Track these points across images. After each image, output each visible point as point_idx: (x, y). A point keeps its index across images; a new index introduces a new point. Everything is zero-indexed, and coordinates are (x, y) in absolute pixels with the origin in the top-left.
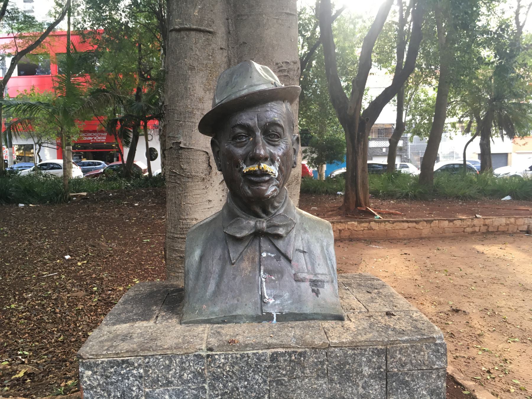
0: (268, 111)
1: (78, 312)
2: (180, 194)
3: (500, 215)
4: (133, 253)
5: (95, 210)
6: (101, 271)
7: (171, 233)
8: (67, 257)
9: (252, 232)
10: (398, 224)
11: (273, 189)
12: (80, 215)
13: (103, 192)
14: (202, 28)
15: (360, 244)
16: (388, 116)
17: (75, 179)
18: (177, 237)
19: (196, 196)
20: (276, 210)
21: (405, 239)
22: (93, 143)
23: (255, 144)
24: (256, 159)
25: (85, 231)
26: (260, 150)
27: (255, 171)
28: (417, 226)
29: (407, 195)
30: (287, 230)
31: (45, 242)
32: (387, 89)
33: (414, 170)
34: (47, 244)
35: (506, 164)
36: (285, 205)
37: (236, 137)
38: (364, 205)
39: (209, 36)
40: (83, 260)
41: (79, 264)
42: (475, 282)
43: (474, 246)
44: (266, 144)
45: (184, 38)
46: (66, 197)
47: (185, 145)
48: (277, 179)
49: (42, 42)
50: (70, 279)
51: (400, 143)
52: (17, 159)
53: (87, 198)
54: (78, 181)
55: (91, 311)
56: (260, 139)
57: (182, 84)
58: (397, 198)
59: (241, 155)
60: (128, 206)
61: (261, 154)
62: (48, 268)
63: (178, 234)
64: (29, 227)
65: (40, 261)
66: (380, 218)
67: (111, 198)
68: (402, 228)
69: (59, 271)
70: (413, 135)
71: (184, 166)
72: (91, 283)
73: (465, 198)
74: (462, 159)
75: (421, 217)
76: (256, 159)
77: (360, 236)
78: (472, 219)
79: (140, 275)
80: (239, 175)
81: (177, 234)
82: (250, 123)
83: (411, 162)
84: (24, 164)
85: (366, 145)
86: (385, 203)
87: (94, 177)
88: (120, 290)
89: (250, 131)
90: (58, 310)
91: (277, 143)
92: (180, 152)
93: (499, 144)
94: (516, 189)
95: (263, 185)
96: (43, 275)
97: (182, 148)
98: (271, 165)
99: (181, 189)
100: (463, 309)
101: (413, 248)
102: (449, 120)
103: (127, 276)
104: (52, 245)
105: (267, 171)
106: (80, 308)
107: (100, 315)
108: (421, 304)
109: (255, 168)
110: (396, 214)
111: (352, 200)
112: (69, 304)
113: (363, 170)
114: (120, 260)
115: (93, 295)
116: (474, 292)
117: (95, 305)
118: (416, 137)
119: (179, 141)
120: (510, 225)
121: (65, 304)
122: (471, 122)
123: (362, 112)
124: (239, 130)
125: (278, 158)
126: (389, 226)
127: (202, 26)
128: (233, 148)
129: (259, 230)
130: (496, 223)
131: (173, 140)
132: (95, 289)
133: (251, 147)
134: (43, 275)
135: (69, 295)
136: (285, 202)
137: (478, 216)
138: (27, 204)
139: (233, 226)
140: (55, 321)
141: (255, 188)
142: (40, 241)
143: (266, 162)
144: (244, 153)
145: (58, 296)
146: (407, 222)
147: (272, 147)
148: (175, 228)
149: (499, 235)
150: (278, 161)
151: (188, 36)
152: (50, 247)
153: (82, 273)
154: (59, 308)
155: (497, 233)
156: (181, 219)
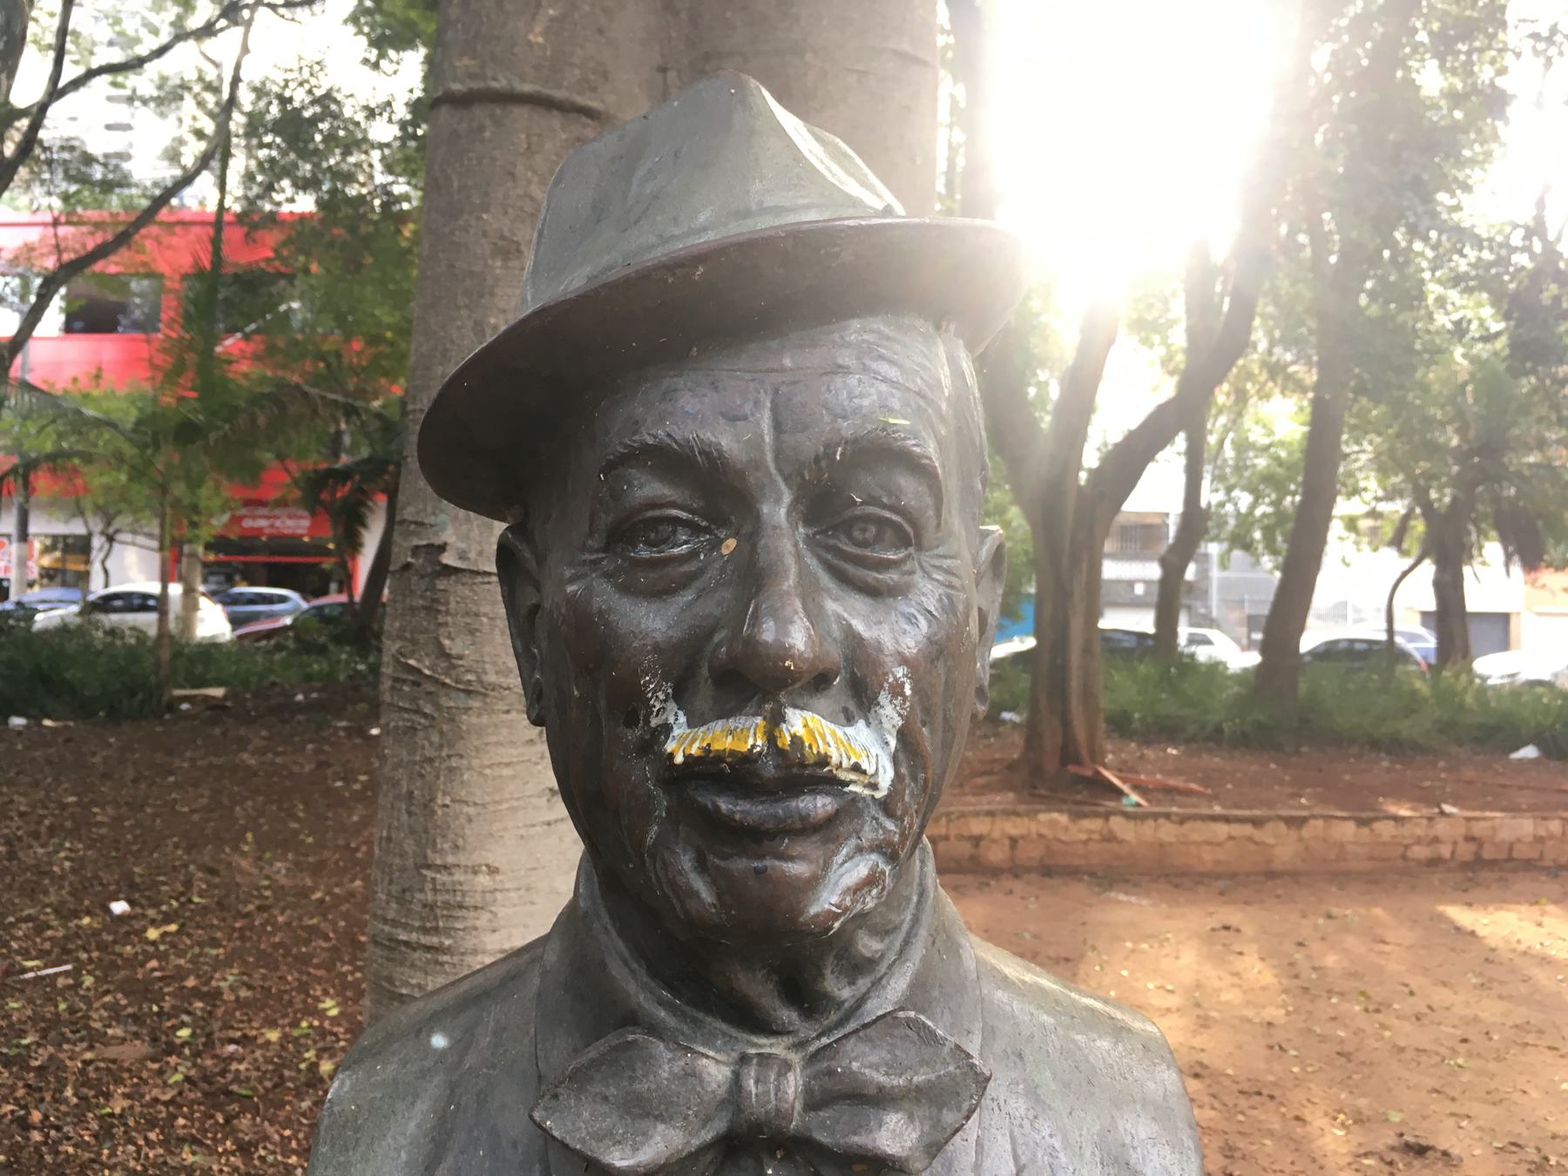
0: (842, 370)
1: (107, 1124)
2: (431, 760)
3: (1513, 809)
4: (339, 901)
5: (243, 743)
6: (218, 964)
7: (385, 921)
8: (119, 907)
9: (707, 1135)
10: (1199, 824)
11: (860, 869)
12: (193, 760)
13: (277, 689)
14: (559, 94)
15: (1079, 889)
16: (1158, 493)
17: (200, 645)
18: (407, 944)
19: (497, 771)
20: (863, 983)
21: (1219, 876)
22: (271, 537)
23: (752, 578)
24: (754, 681)
25: (196, 817)
26: (783, 625)
27: (748, 759)
28: (1258, 834)
29: (1219, 730)
30: (936, 1124)
31: (61, 847)
32: (1161, 410)
33: (1231, 653)
34: (67, 858)
35: (1504, 644)
36: (918, 951)
37: (629, 531)
38: (1087, 760)
39: (585, 126)
40: (167, 919)
41: (153, 934)
42: (1465, 1041)
43: (1441, 908)
44: (825, 579)
45: (482, 129)
46: (159, 702)
47: (462, 556)
48: (887, 806)
49: (137, 237)
50: (107, 992)
51: (1190, 573)
52: (42, 576)
53: (224, 708)
54: (211, 649)
55: (152, 1124)
56: (787, 546)
57: (464, 312)
58: (1188, 741)
59: (657, 648)
60: (349, 736)
61: (787, 652)
62: (47, 945)
63: (412, 929)
64: (24, 795)
65: (29, 919)
66: (1138, 805)
67: (300, 708)
68: (1211, 838)
69: (77, 960)
70: (1229, 551)
71: (454, 646)
72: (176, 1011)
73: (1396, 747)
74: (1384, 625)
75: (1270, 804)
76: (754, 681)
77: (1076, 862)
78: (1430, 819)
79: (345, 985)
80: (645, 771)
81: (406, 927)
82: (727, 441)
83: (1219, 627)
84: (55, 593)
85: (1096, 569)
86: (1150, 753)
87: (258, 640)
88: (268, 1043)
89: (721, 494)
90: (36, 1116)
91: (892, 577)
92: (441, 584)
93: (1491, 581)
94: (1553, 725)
95: (797, 849)
96: (25, 970)
97: (449, 571)
98: (849, 720)
99: (435, 738)
100: (1442, 1143)
101: (1249, 908)
102: (1343, 507)
103: (303, 988)
104: (82, 859)
105: (824, 761)
106: (117, 1111)
107: (181, 1140)
108: (1297, 1118)
109: (743, 736)
110: (1189, 793)
111: (1051, 741)
112: (85, 1091)
113: (1087, 650)
114: (288, 924)
115: (173, 1060)
116: (1466, 1077)
117: (172, 1101)
118: (1237, 554)
119: (437, 541)
120: (1550, 843)
121: (69, 1092)
122: (1406, 518)
123: (1083, 476)
124: (648, 488)
125: (900, 672)
126: (1167, 832)
127: (559, 87)
128: (605, 596)
129: (757, 1127)
130: (1505, 835)
131: (416, 534)
132: (184, 1033)
133: (727, 594)
134: (25, 970)
135: (89, 1056)
136: (916, 921)
137: (1447, 808)
138: (35, 718)
139: (597, 1088)
140: (18, 1161)
141: (740, 865)
142: (42, 846)
143: (822, 702)
144: (676, 634)
145: (51, 1057)
146: (1227, 820)
147: (860, 603)
148: (401, 901)
149: (1515, 871)
150: (896, 691)
151: (498, 123)
152: (73, 870)
153: (154, 970)
154: (43, 1106)
155: (1512, 865)
156: (429, 867)
